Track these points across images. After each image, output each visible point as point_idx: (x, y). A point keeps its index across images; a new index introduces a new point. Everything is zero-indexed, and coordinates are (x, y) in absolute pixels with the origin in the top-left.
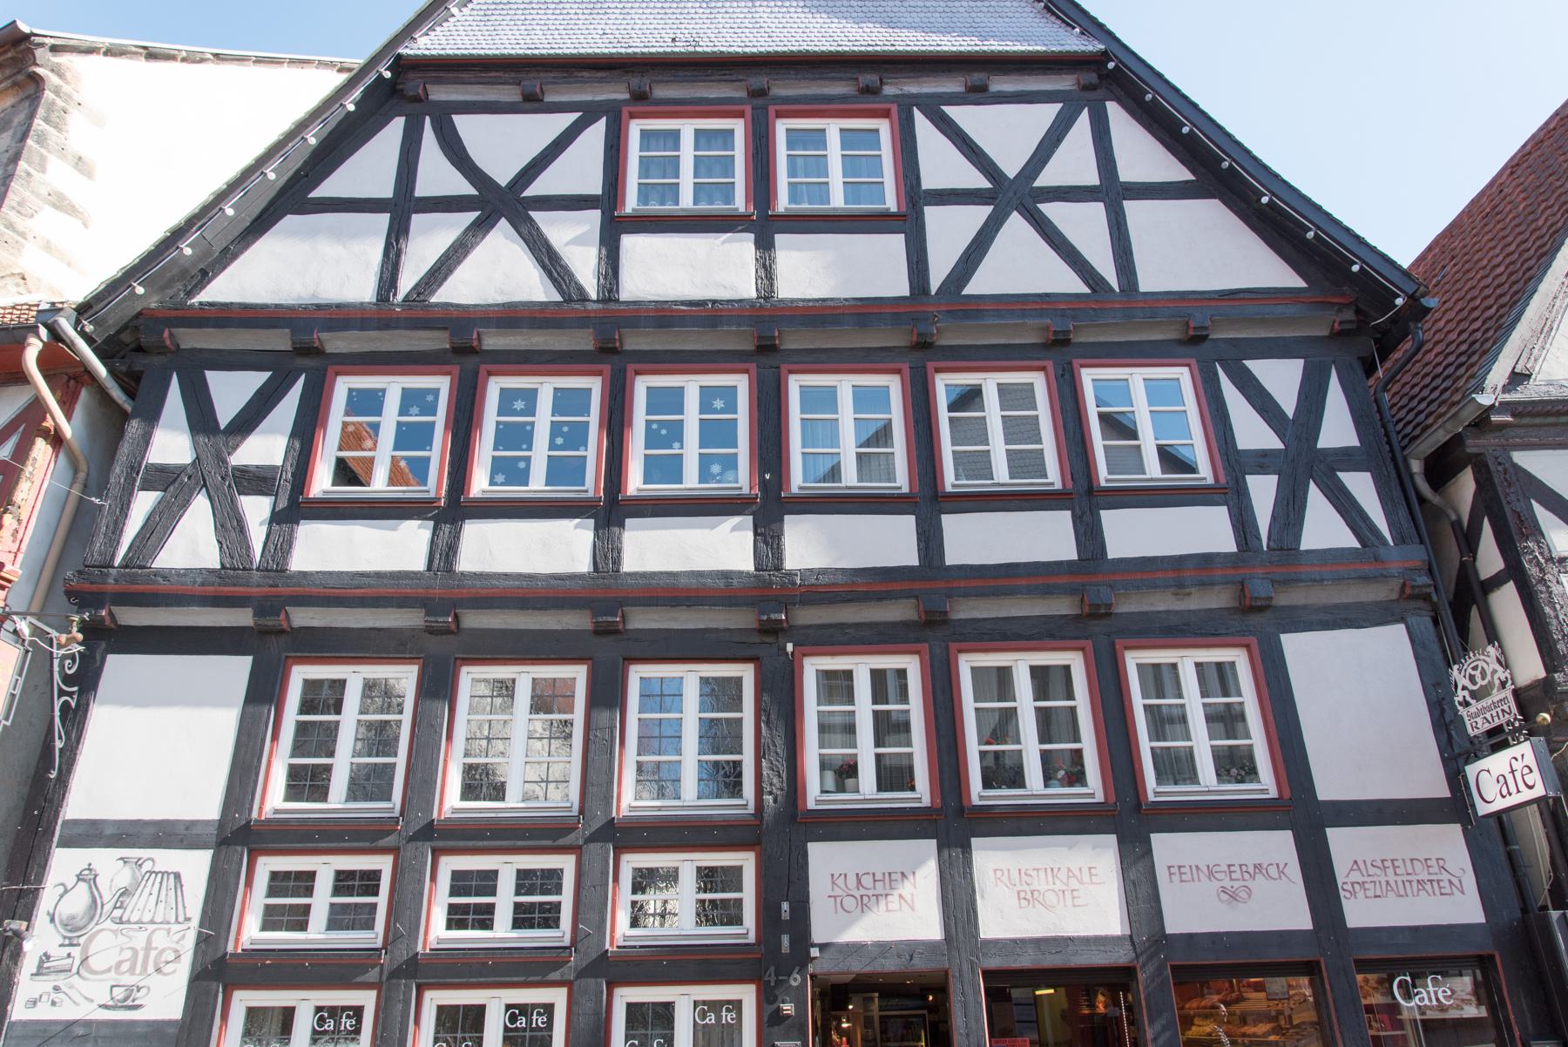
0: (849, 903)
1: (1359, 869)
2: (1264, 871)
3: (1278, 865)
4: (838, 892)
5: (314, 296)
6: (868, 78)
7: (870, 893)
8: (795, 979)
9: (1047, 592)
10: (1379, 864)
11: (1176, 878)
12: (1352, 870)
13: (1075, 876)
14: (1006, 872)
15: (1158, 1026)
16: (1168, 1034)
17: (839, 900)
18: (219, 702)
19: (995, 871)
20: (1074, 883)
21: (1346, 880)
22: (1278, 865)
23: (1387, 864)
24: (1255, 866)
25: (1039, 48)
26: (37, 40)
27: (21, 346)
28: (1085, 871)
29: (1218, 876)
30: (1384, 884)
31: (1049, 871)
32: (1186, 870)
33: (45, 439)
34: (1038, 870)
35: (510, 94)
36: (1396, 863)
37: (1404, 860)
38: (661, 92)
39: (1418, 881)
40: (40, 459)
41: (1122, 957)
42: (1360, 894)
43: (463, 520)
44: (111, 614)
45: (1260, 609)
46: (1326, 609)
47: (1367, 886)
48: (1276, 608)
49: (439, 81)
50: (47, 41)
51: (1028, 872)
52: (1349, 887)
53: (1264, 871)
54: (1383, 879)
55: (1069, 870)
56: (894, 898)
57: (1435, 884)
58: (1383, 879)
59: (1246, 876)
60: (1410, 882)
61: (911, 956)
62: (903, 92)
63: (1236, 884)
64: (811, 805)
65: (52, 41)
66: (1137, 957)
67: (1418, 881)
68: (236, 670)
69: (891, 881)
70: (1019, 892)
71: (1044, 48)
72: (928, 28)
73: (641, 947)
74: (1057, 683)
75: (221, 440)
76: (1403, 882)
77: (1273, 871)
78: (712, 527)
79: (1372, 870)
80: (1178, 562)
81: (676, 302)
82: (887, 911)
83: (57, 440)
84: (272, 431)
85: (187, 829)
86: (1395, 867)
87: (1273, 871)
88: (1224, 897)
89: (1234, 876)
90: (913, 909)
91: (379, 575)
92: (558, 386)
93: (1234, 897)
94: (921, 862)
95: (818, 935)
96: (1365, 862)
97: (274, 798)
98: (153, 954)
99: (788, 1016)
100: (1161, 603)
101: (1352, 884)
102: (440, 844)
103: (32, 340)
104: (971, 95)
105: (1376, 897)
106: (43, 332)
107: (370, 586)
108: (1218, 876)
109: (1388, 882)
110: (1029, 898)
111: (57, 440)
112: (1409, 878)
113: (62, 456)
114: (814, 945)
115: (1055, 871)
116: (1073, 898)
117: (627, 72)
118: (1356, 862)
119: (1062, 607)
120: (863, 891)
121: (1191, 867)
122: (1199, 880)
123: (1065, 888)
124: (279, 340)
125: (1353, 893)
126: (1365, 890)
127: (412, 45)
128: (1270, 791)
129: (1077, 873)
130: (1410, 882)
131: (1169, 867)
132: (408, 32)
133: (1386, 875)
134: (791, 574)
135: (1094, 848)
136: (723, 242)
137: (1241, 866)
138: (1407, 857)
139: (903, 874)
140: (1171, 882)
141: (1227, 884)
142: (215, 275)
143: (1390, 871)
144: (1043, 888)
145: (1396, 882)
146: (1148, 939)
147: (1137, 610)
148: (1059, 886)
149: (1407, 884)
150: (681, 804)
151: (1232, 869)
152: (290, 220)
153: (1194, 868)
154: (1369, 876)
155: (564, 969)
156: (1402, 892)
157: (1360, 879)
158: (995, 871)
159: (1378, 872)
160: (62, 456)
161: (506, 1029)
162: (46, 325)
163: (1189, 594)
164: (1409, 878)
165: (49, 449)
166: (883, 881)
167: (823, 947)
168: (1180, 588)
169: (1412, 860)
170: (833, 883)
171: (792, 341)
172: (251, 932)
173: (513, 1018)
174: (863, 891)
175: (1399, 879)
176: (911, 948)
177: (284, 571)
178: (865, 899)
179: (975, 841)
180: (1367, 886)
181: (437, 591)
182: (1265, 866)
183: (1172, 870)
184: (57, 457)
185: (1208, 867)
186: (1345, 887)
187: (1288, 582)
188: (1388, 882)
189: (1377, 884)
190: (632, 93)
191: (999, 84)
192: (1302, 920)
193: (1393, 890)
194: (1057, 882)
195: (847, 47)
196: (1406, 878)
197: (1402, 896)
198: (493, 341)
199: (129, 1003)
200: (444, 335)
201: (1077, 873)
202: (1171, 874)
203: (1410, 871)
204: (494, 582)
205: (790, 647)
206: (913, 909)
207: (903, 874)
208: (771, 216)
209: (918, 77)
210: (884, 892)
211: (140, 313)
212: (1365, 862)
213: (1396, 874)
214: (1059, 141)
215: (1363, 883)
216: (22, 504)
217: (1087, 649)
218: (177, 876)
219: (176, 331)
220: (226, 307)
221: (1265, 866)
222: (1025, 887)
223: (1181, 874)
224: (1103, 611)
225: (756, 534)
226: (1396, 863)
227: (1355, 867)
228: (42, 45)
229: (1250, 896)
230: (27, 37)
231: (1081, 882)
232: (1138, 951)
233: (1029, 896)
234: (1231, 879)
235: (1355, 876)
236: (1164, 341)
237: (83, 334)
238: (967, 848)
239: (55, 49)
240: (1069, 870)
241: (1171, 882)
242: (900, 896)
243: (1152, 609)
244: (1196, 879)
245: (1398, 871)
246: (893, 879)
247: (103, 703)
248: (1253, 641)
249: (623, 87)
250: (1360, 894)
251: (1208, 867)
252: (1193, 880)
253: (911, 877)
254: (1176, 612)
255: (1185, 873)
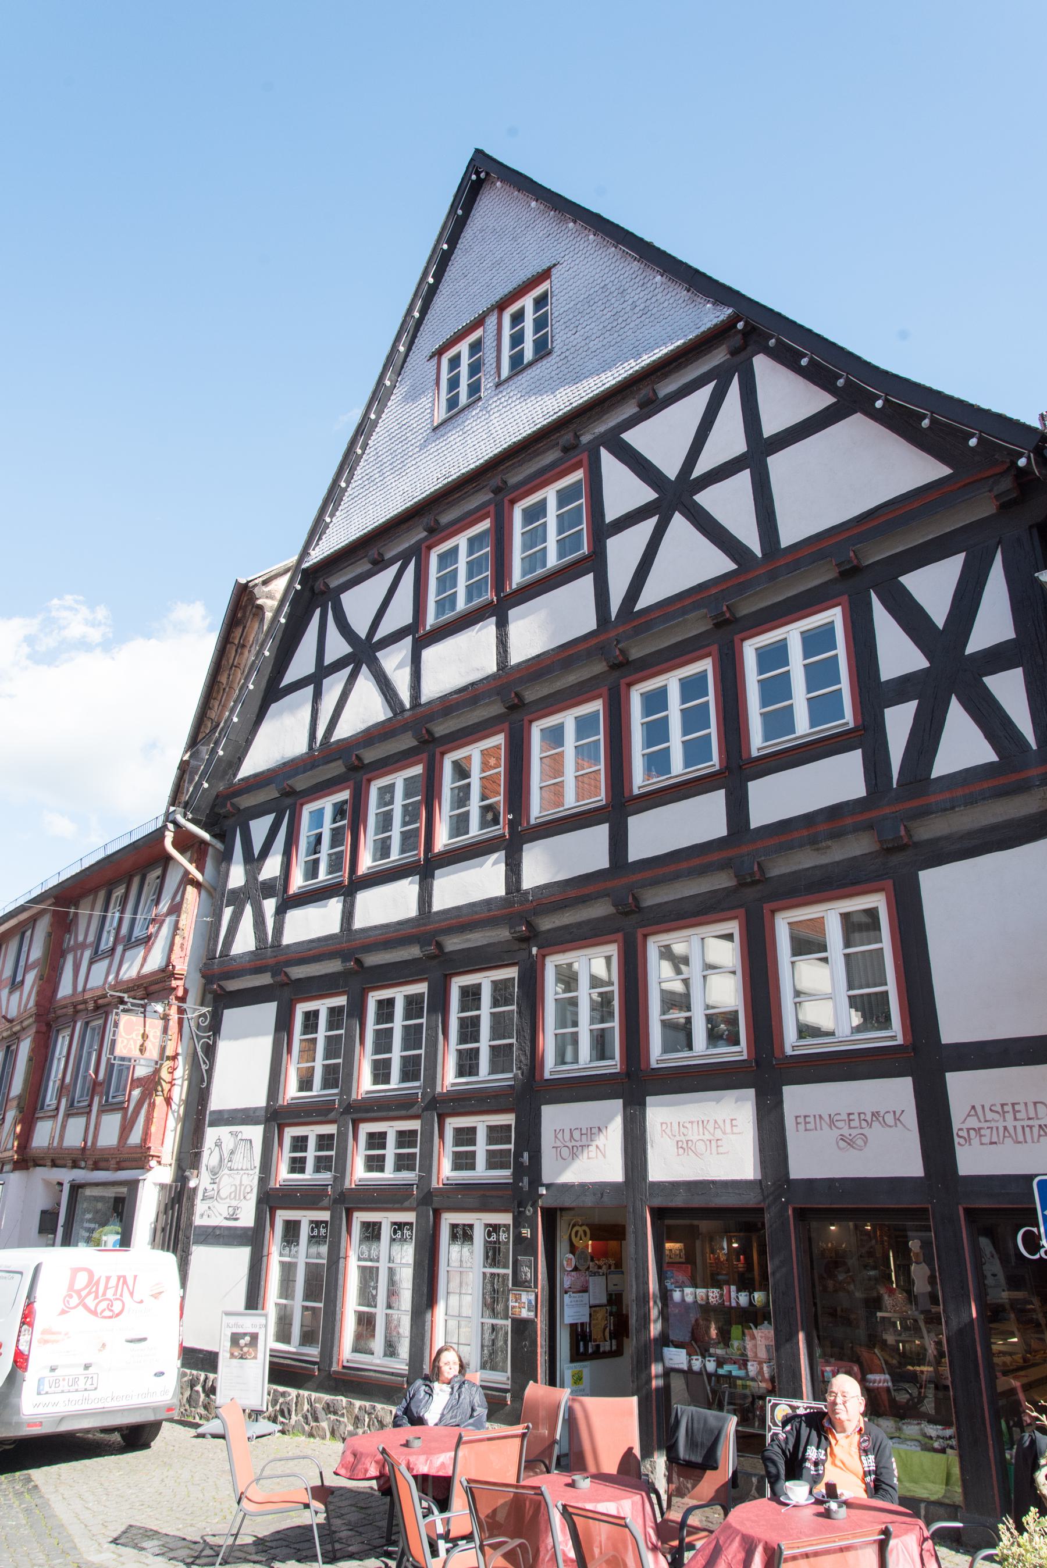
0: (565, 1152)
1: (976, 1114)
2: (881, 1119)
3: (894, 1112)
4: (558, 1144)
5: (283, 757)
6: (567, 437)
7: (578, 1144)
8: (529, 1211)
9: (703, 871)
10: (998, 1108)
11: (801, 1127)
12: (968, 1115)
13: (719, 1127)
14: (669, 1125)
15: (777, 1262)
16: (784, 1270)
17: (559, 1149)
18: (259, 1033)
19: (662, 1124)
20: (718, 1134)
21: (961, 1126)
22: (894, 1112)
23: (1006, 1108)
24: (873, 1114)
25: (679, 343)
26: (251, 584)
27: (163, 837)
28: (728, 1122)
29: (838, 1124)
30: (1001, 1130)
31: (700, 1123)
32: (810, 1119)
33: (192, 885)
34: (692, 1122)
35: (364, 566)
36: (1017, 1107)
37: (1026, 1104)
38: (445, 519)
39: (1040, 1126)
40: (189, 899)
41: (751, 1200)
42: (975, 1141)
43: (356, 892)
44: (219, 986)
45: (902, 848)
46: (970, 834)
47: (983, 1132)
48: (916, 845)
49: (330, 574)
50: (256, 581)
51: (685, 1125)
52: (964, 1134)
53: (881, 1119)
54: (1001, 1125)
55: (716, 1122)
56: (593, 1148)
57: (714, 1143)
58: (1001, 1125)
59: (864, 1124)
60: (1031, 1127)
61: (602, 1194)
62: (596, 435)
63: (854, 1132)
64: (547, 1075)
65: (261, 579)
66: (764, 1200)
67: (1040, 1126)
68: (268, 1011)
69: (591, 1134)
70: (677, 1142)
71: (682, 341)
72: (606, 367)
73: (456, 1184)
74: (806, 933)
75: (255, 864)
76: (1023, 1127)
77: (890, 1119)
78: (481, 866)
79: (990, 1115)
80: (808, 819)
81: (451, 694)
82: (588, 1158)
83: (197, 884)
84: (274, 854)
85: (254, 1113)
86: (1015, 1112)
87: (890, 1119)
88: (842, 1144)
89: (853, 1124)
90: (604, 1156)
91: (319, 940)
92: (406, 777)
93: (850, 1143)
94: (611, 1119)
95: (546, 1179)
96: (983, 1107)
97: (291, 1091)
98: (243, 1187)
99: (526, 1238)
100: (805, 860)
101: (968, 1130)
102: (355, 1116)
103: (167, 833)
104: (644, 410)
105: (992, 1143)
106: (171, 826)
107: (315, 948)
108: (838, 1124)
109: (1005, 1128)
110: (684, 1147)
111: (197, 884)
112: (1030, 1123)
113: (203, 892)
114: (543, 1185)
115: (705, 1123)
116: (718, 1146)
117: (422, 515)
118: (973, 1107)
119: (723, 881)
120: (574, 1143)
121: (815, 1116)
122: (821, 1129)
123: (711, 1137)
124: (269, 794)
125: (968, 1140)
126: (981, 1136)
127: (310, 558)
128: (898, 1038)
129: (722, 1125)
130: (1031, 1127)
131: (797, 1117)
132: (305, 553)
133: (1005, 1120)
134: (527, 892)
135: (736, 1102)
136: (477, 632)
137: (859, 1114)
138: (1031, 1099)
139: (599, 1128)
140: (798, 1131)
141: (846, 1132)
142: (244, 758)
143: (1010, 1116)
144: (695, 1138)
145: (1015, 1127)
146: (774, 1184)
147: (788, 871)
148: (708, 1136)
149: (1027, 1130)
150: (576, 1067)
151: (851, 1117)
152: (274, 707)
153: (817, 1118)
154: (986, 1121)
155: (411, 1199)
156: (1021, 1138)
157: (977, 1125)
158: (662, 1124)
159: (996, 1116)
160: (203, 892)
161: (486, 1242)
162: (172, 822)
163: (829, 847)
164: (1030, 1123)
165: (195, 890)
166: (586, 1134)
167: (548, 1186)
168: (813, 842)
169: (1035, 1103)
170: (556, 1137)
171: (531, 695)
172: (283, 1174)
173: (489, 1235)
174: (574, 1143)
175: (1019, 1124)
176: (601, 1189)
177: (280, 945)
178: (575, 1148)
179: (649, 1099)
180: (983, 1132)
181: (344, 945)
182: (882, 1115)
183: (799, 1120)
184: (200, 893)
185: (830, 1115)
186: (960, 1133)
187: (924, 813)
188: (1005, 1128)
189: (995, 1130)
190: (493, 492)
191: (666, 388)
192: (913, 1167)
193: (1010, 1136)
194: (706, 1132)
195: (542, 422)
196: (1026, 1123)
197: (995, 1143)
198: (370, 756)
199: (234, 1217)
200: (340, 762)
201: (722, 1125)
202: (797, 1123)
203: (1032, 1114)
204: (370, 933)
205: (534, 950)
206: (604, 1156)
207: (599, 1128)
208: (505, 596)
209: (600, 418)
210: (587, 1144)
211: (217, 796)
212: (983, 1107)
213: (1015, 1119)
214: (712, 423)
215: (980, 1129)
216: (183, 927)
217: (645, 933)
218: (251, 1141)
219: (235, 800)
220: (255, 776)
221: (882, 1115)
222: (683, 1138)
223: (806, 1123)
224: (749, 880)
225: (507, 865)
226: (1017, 1107)
227: (973, 1113)
228: (256, 585)
229: (865, 1143)
230: (246, 586)
231: (724, 1133)
232: (766, 1193)
233: (685, 1146)
234: (850, 1128)
235: (972, 1122)
236: (826, 583)
237: (188, 820)
238: (643, 1105)
239: (265, 583)
240: (716, 1122)
241: (798, 1131)
242: (597, 1147)
243: (801, 867)
244: (818, 1127)
245: (1018, 1116)
246: (593, 1131)
247: (224, 1039)
248: (640, 932)
249: (421, 528)
250: (975, 1141)
251: (830, 1115)
252: (816, 1129)
253: (604, 1131)
254: (821, 866)
255: (809, 1123)
